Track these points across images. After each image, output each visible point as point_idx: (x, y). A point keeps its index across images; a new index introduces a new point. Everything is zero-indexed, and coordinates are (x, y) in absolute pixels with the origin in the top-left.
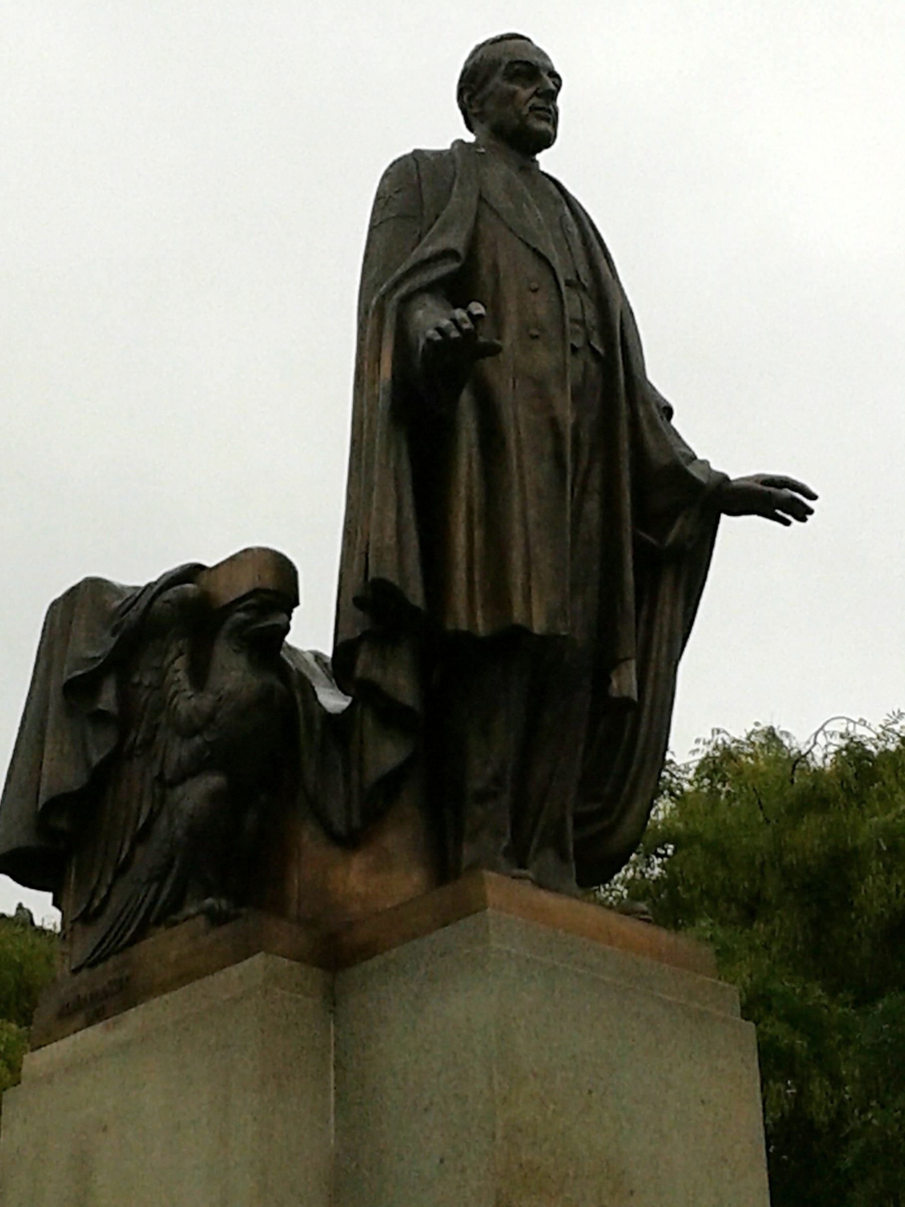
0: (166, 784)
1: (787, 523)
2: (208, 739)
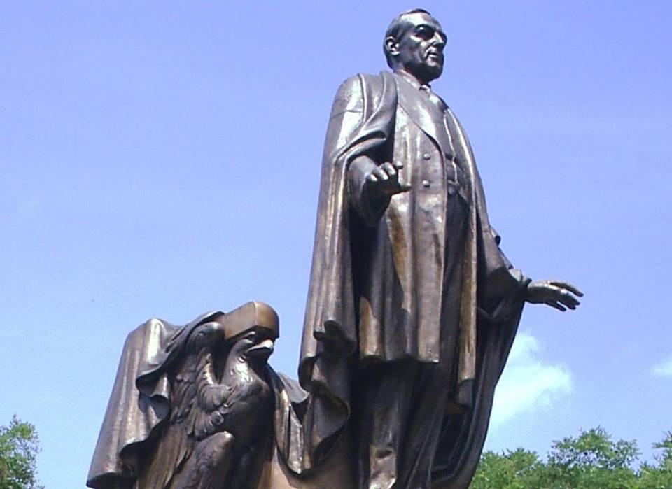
0: (194, 439)
1: (564, 310)
2: (223, 412)
